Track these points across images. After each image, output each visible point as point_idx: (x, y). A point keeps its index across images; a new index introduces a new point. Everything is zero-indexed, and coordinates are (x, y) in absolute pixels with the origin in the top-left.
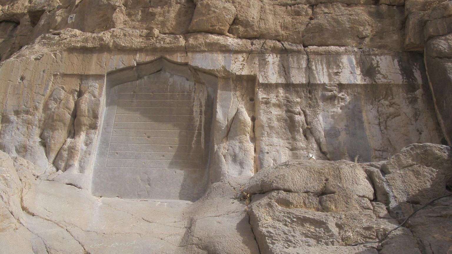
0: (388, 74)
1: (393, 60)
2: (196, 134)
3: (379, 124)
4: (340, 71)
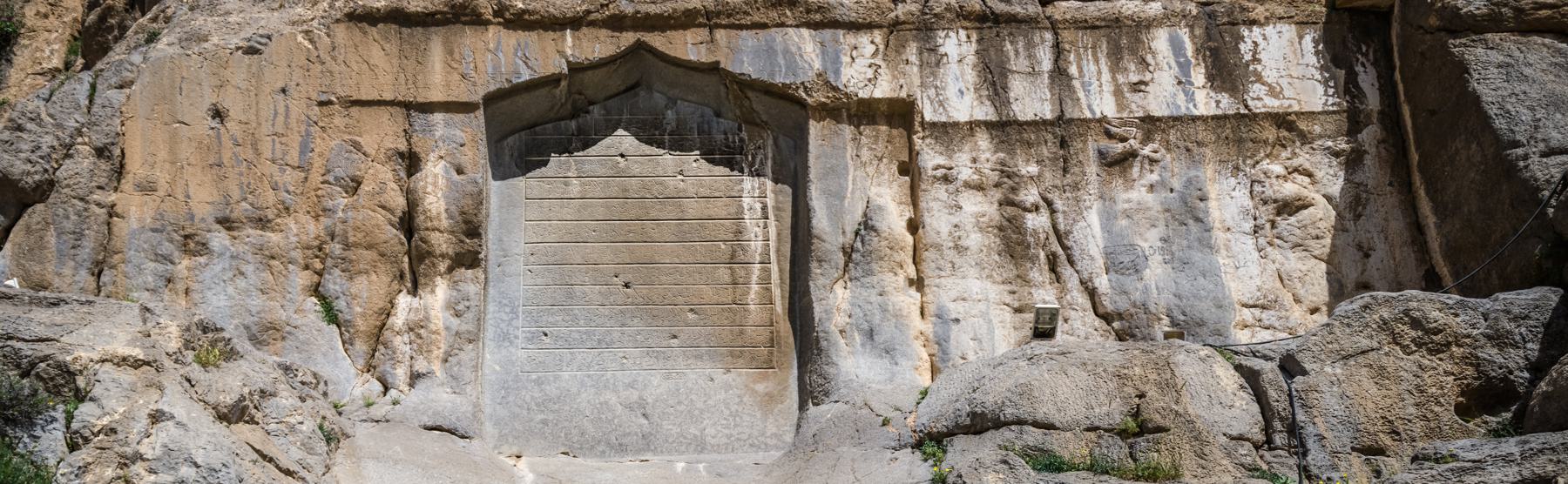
0: (1284, 82)
1: (1301, 38)
2: (757, 272)
3: (1256, 230)
4: (1148, 77)
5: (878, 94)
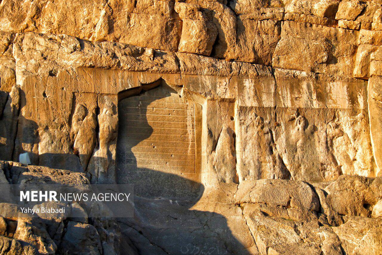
1: (343, 86)
2: (190, 145)
4: (300, 96)
5: (226, 97)
